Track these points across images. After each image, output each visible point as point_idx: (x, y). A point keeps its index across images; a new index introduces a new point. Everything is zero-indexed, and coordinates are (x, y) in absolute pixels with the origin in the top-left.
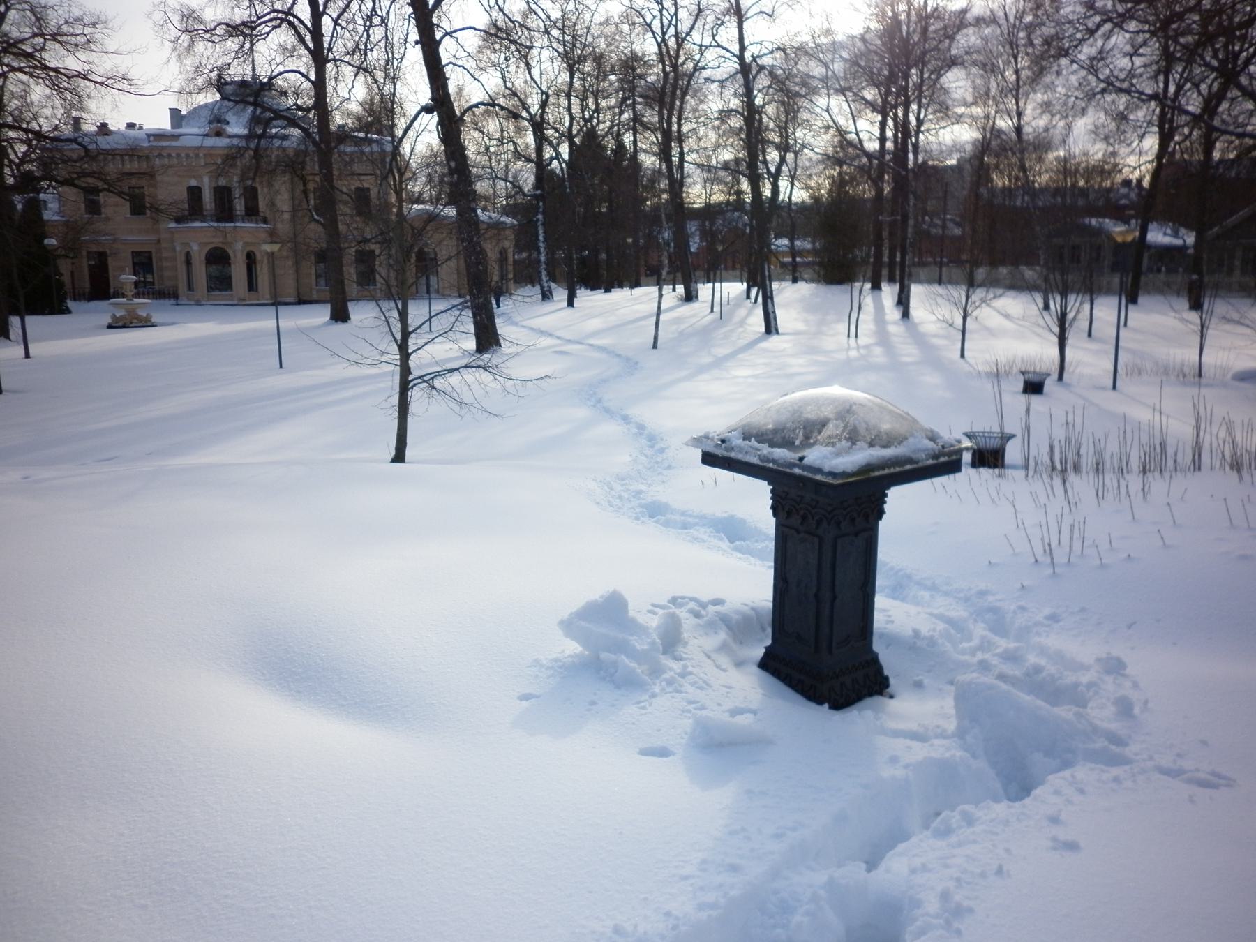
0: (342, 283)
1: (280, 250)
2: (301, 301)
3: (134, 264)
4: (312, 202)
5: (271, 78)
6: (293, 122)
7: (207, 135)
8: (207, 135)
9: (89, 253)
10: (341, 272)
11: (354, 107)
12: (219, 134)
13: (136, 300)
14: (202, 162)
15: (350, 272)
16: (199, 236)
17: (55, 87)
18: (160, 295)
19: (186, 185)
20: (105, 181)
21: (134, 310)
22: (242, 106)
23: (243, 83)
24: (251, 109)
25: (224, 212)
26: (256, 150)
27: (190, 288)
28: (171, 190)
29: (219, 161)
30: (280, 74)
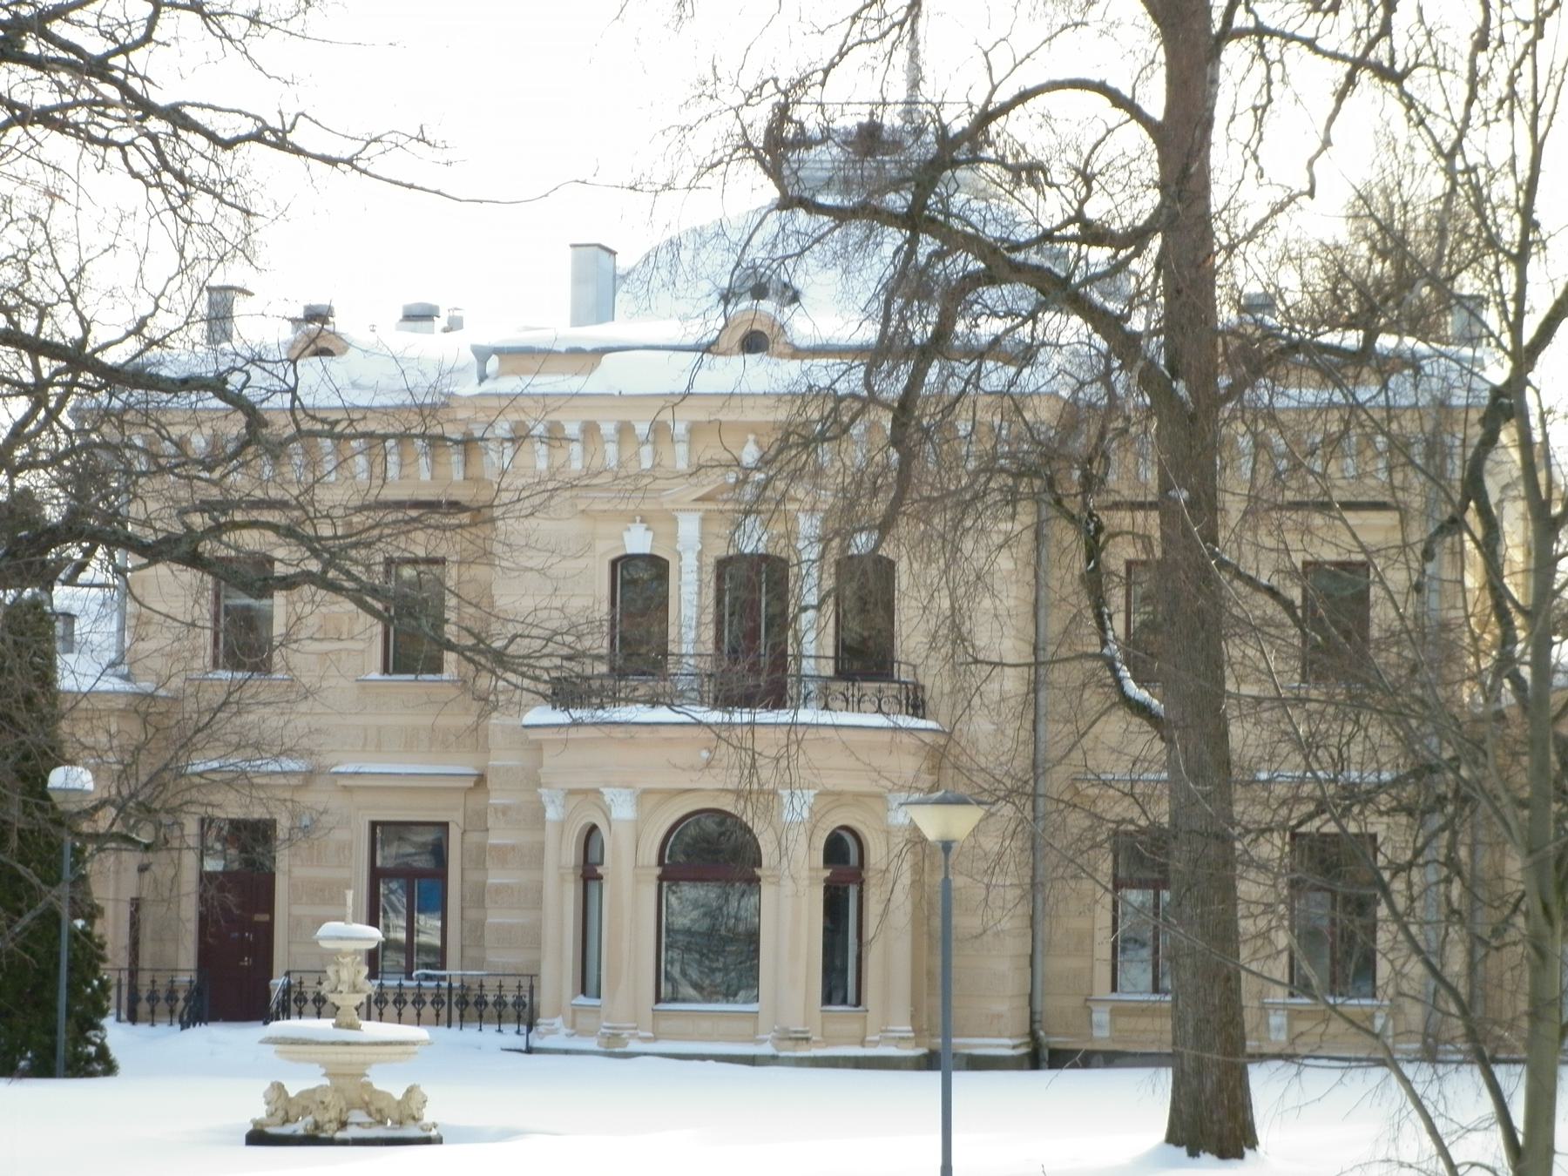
0: (1229, 983)
1: (976, 831)
2: (1041, 1055)
3: (377, 875)
4: (1118, 626)
5: (985, 118)
6: (1060, 292)
7: (707, 348)
8: (707, 348)
9: (205, 823)
10: (1225, 935)
11: (1327, 223)
12: (754, 343)
13: (374, 1030)
14: (680, 458)
15: (1267, 943)
16: (642, 768)
17: (171, 178)
18: (466, 1006)
19: (607, 551)
20: (314, 545)
21: (356, 1074)
22: (856, 230)
23: (869, 138)
24: (893, 239)
25: (753, 666)
26: (904, 408)
27: (586, 983)
28: (547, 582)
29: (750, 455)
30: (1023, 97)
